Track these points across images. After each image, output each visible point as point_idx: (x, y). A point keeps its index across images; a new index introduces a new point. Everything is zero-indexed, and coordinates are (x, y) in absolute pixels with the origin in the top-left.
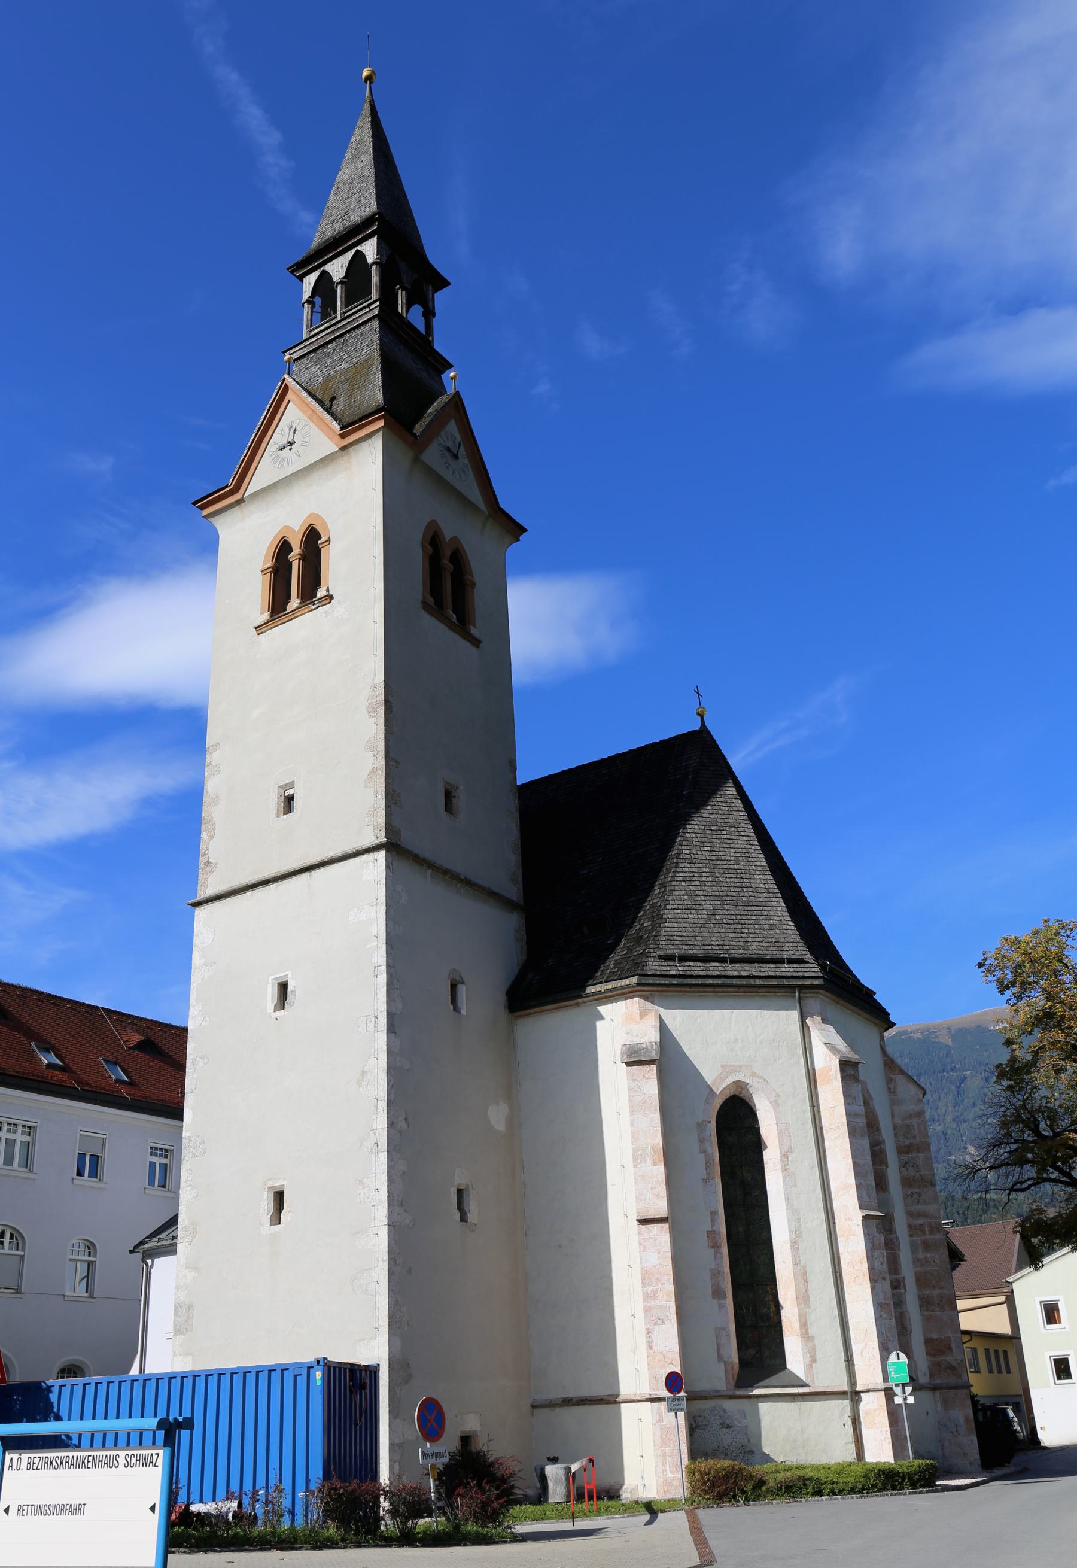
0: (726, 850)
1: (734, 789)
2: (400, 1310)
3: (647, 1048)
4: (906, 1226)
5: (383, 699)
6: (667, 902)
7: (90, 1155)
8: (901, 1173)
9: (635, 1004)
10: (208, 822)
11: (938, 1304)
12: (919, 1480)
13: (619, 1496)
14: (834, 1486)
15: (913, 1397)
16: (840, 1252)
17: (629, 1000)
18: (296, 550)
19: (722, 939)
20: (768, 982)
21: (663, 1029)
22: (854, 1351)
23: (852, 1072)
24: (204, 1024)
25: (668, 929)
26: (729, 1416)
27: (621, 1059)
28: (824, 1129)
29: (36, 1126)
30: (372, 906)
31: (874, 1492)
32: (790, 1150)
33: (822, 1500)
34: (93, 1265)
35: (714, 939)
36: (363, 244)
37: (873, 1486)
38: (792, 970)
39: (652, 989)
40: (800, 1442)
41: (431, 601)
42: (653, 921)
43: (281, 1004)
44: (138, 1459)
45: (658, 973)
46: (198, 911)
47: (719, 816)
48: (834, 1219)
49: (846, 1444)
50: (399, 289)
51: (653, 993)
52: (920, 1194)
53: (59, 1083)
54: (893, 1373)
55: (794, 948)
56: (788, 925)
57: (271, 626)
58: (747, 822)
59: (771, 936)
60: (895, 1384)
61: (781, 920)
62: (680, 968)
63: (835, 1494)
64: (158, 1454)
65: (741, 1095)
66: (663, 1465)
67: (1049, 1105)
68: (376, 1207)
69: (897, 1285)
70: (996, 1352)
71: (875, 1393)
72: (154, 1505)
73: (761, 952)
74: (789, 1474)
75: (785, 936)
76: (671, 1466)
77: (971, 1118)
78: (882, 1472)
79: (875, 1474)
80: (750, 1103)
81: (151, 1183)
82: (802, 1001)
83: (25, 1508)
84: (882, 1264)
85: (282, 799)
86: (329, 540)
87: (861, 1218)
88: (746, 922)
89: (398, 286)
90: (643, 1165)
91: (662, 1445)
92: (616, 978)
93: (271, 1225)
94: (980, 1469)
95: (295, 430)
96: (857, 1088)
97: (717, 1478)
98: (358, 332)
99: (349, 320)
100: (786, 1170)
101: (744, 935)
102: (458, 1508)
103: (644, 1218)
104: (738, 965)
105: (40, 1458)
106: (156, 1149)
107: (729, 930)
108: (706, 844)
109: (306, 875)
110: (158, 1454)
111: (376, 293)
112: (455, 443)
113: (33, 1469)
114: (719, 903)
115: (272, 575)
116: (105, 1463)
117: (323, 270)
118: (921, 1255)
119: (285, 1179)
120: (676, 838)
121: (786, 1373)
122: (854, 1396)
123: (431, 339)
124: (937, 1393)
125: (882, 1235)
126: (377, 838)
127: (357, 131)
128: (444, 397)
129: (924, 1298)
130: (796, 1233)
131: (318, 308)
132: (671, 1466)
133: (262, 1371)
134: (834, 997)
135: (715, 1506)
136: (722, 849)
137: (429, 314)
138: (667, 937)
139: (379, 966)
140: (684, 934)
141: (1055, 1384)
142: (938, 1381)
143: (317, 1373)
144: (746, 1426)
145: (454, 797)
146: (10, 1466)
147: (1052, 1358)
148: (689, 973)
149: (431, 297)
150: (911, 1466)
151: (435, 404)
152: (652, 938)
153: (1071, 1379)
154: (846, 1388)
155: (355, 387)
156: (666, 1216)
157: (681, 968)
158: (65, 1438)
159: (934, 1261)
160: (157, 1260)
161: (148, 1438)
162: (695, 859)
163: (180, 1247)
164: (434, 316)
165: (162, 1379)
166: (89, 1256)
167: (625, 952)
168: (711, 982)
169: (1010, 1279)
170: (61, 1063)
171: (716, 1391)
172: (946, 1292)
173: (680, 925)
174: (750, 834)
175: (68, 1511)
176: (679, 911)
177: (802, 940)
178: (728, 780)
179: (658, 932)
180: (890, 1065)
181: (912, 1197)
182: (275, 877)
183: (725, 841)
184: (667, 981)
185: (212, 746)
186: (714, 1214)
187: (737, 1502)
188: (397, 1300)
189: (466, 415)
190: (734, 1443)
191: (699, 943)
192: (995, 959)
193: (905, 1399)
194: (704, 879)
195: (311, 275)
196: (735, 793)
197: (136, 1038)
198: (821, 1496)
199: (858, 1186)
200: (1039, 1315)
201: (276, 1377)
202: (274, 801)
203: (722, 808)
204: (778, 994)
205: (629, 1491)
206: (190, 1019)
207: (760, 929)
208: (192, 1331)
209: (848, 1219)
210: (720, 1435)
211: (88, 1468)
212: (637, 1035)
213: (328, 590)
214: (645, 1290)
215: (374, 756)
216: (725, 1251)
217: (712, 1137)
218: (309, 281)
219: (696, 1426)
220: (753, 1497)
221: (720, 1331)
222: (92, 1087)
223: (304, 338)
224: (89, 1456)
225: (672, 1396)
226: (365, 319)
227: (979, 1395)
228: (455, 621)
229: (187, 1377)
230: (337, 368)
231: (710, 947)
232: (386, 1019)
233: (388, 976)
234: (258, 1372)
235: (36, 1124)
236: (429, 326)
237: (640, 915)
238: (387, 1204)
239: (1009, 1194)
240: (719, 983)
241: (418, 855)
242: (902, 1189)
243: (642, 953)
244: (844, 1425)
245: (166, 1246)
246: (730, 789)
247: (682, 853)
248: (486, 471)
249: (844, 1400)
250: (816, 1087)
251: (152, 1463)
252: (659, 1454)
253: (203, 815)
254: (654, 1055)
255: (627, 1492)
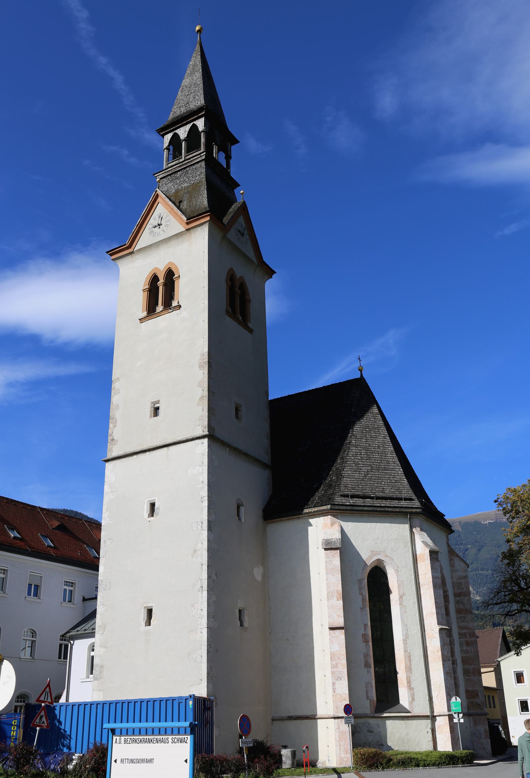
0: (373, 441)
1: (377, 410)
2: (212, 670)
3: (335, 541)
4: (458, 633)
5: (207, 360)
6: (344, 467)
7: (34, 585)
8: (455, 607)
9: (328, 519)
10: (113, 418)
11: (473, 673)
12: (465, 760)
13: (316, 766)
14: (425, 762)
15: (463, 719)
16: (427, 646)
17: (325, 517)
18: (161, 281)
19: (372, 487)
20: (394, 509)
21: (343, 532)
22: (433, 696)
23: (435, 556)
24: (110, 522)
25: (345, 481)
26: (371, 726)
27: (322, 547)
28: (421, 584)
29: (8, 570)
30: (201, 466)
31: (444, 766)
32: (404, 594)
33: (419, 769)
34: (34, 642)
35: (367, 487)
36: (197, 121)
37: (444, 763)
38: (406, 504)
39: (337, 511)
40: (406, 741)
41: (230, 310)
42: (337, 477)
43: (151, 513)
44: (178, 739)
45: (341, 503)
46: (107, 464)
47: (370, 423)
48: (424, 629)
49: (428, 742)
50: (214, 144)
51: (338, 514)
52: (465, 617)
53: (19, 547)
54: (453, 707)
55: (407, 493)
56: (404, 480)
57: (148, 319)
58: (384, 427)
59: (396, 486)
60: (454, 713)
61: (400, 478)
62: (351, 501)
63: (425, 766)
64: (187, 738)
65: (380, 566)
66: (340, 750)
67: (528, 574)
68: (201, 618)
69: (454, 663)
70: (489, 696)
71: (444, 717)
72: (187, 760)
73: (391, 494)
74: (403, 756)
75: (403, 486)
76: (344, 751)
77: (470, 571)
78: (448, 756)
79: (445, 757)
80: (384, 570)
81: (64, 600)
82: (411, 520)
83: (124, 760)
84: (448, 652)
85: (153, 409)
86: (179, 276)
87: (439, 630)
88: (383, 478)
89: (214, 143)
90: (332, 600)
91: (339, 741)
92: (319, 505)
93: (145, 626)
94: (491, 756)
95: (162, 218)
96: (437, 564)
97: (369, 756)
98: (194, 167)
99: (189, 161)
100: (401, 604)
101: (382, 485)
102: (257, 769)
103: (332, 627)
104: (380, 501)
105: (130, 738)
106: (67, 582)
107: (375, 483)
108: (363, 438)
109: (166, 449)
110: (187, 738)
111: (203, 147)
112: (242, 227)
113: (127, 743)
114: (370, 468)
115: (148, 292)
116: (162, 741)
117: (175, 132)
118: (465, 648)
119: (153, 603)
120: (349, 434)
121: (400, 706)
122: (433, 718)
123: (229, 171)
124: (471, 717)
125: (448, 638)
126: (204, 432)
127: (193, 59)
128: (237, 203)
129: (465, 670)
130: (406, 636)
131: (171, 152)
132: (344, 751)
133: (162, 700)
134: (426, 518)
135: (368, 771)
136: (371, 441)
137: (228, 158)
138: (344, 485)
139: (204, 497)
140: (353, 484)
141: (520, 714)
142: (472, 712)
143: (190, 702)
144: (380, 732)
145: (240, 410)
146: (116, 742)
147: (519, 701)
148: (356, 504)
149: (229, 148)
150: (462, 753)
151: (233, 207)
152: (337, 485)
153: (529, 711)
154: (429, 714)
155: (192, 196)
156: (343, 626)
157: (351, 501)
158: (63, 732)
159: (471, 651)
160: (76, 641)
161: (182, 731)
162: (358, 445)
163: (97, 635)
164: (231, 159)
165: (112, 703)
166: (33, 637)
167: (323, 492)
168: (367, 509)
169: (499, 660)
170: (20, 537)
171: (366, 714)
172: (477, 667)
173: (351, 479)
174: (385, 433)
175: (145, 762)
176: (350, 472)
177: (411, 489)
178: (374, 404)
179: (340, 482)
180: (451, 552)
181: (461, 619)
182: (149, 449)
183: (373, 436)
184: (345, 508)
185: (116, 379)
186: (366, 625)
187: (378, 769)
188: (211, 665)
189: (248, 213)
190: (374, 740)
191: (360, 489)
192: (504, 499)
193: (459, 720)
194: (362, 456)
195: (168, 134)
196: (378, 412)
197: (56, 523)
198: (419, 767)
199: (437, 613)
200: (513, 678)
201: (169, 703)
202: (148, 410)
203: (371, 419)
204: (399, 516)
205: (321, 763)
206: (102, 519)
207: (390, 482)
208: (103, 679)
209: (432, 629)
210: (367, 736)
211: (154, 743)
212: (330, 535)
213: (178, 303)
214: (332, 663)
215: (202, 390)
216: (371, 644)
217: (365, 587)
218: (167, 138)
219: (355, 731)
220: (386, 767)
221: (368, 684)
222: (36, 549)
223: (164, 168)
224: (154, 738)
225: (347, 716)
226: (197, 161)
227: (490, 719)
228: (241, 320)
229: (125, 702)
230: (183, 186)
231: (366, 491)
232: (207, 524)
233: (209, 502)
234: (160, 701)
235: (7, 568)
236: (228, 164)
237: (330, 473)
238: (207, 617)
239: (505, 618)
240: (371, 509)
241: (223, 441)
242: (456, 615)
243: (332, 493)
244: (428, 732)
245: (82, 634)
246: (375, 409)
247: (352, 442)
248: (257, 242)
249: (428, 720)
250: (417, 563)
251: (185, 741)
252: (338, 745)
253: (110, 415)
254: (338, 545)
255: (320, 764)
